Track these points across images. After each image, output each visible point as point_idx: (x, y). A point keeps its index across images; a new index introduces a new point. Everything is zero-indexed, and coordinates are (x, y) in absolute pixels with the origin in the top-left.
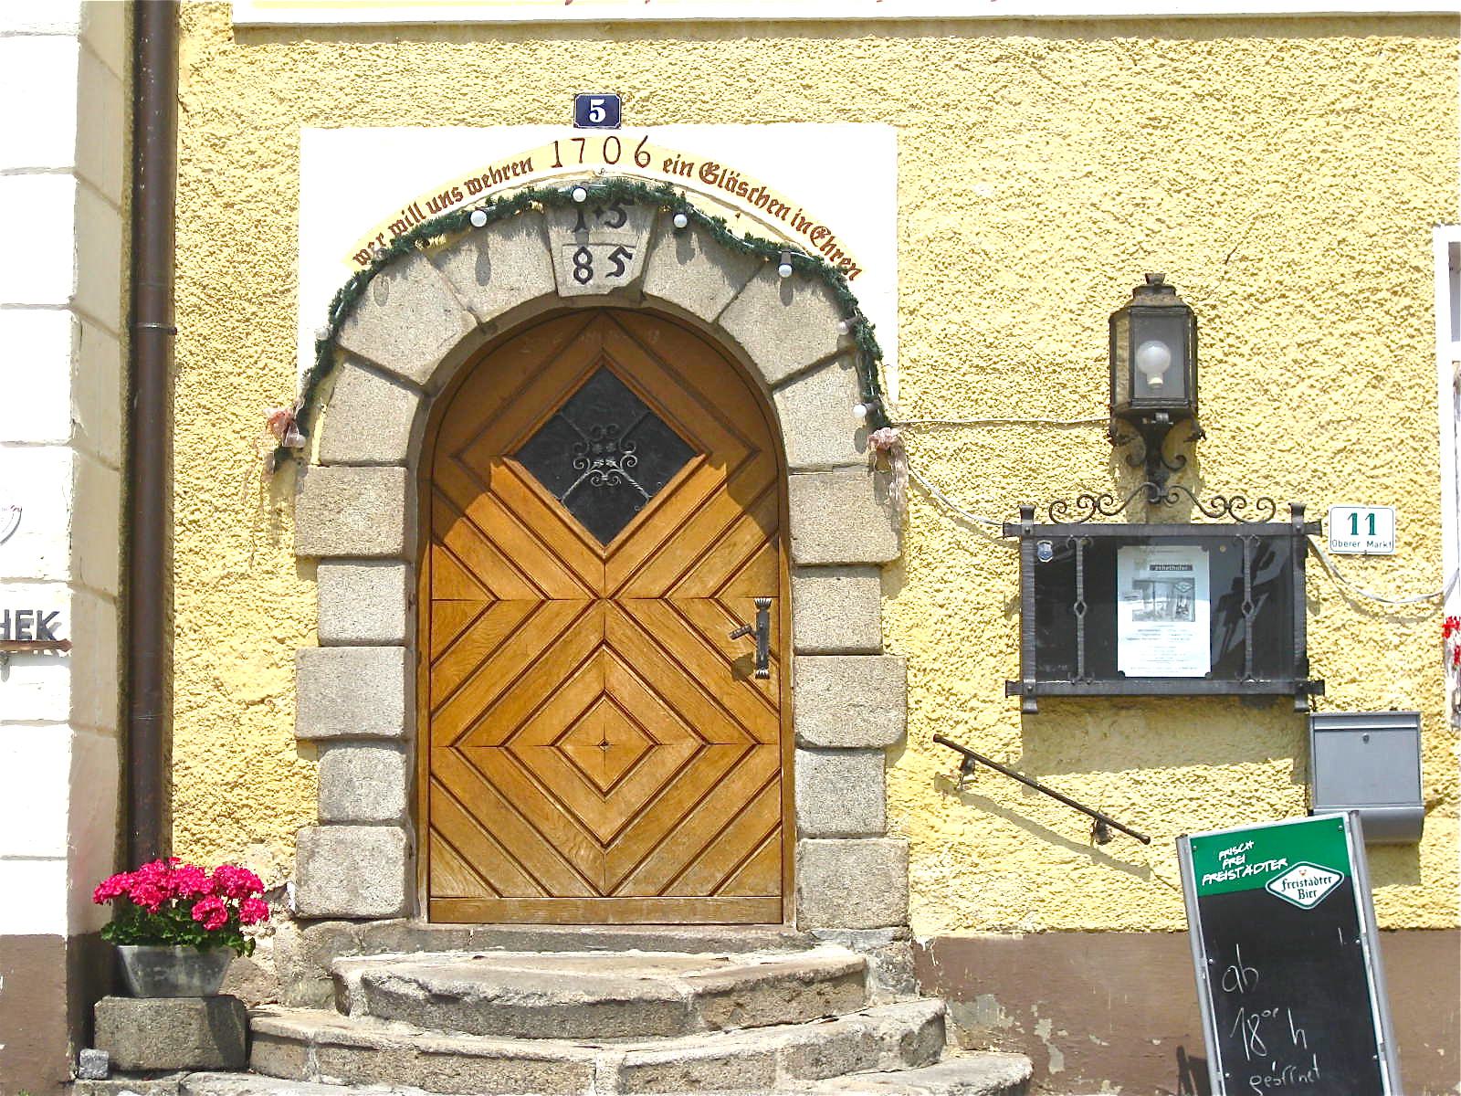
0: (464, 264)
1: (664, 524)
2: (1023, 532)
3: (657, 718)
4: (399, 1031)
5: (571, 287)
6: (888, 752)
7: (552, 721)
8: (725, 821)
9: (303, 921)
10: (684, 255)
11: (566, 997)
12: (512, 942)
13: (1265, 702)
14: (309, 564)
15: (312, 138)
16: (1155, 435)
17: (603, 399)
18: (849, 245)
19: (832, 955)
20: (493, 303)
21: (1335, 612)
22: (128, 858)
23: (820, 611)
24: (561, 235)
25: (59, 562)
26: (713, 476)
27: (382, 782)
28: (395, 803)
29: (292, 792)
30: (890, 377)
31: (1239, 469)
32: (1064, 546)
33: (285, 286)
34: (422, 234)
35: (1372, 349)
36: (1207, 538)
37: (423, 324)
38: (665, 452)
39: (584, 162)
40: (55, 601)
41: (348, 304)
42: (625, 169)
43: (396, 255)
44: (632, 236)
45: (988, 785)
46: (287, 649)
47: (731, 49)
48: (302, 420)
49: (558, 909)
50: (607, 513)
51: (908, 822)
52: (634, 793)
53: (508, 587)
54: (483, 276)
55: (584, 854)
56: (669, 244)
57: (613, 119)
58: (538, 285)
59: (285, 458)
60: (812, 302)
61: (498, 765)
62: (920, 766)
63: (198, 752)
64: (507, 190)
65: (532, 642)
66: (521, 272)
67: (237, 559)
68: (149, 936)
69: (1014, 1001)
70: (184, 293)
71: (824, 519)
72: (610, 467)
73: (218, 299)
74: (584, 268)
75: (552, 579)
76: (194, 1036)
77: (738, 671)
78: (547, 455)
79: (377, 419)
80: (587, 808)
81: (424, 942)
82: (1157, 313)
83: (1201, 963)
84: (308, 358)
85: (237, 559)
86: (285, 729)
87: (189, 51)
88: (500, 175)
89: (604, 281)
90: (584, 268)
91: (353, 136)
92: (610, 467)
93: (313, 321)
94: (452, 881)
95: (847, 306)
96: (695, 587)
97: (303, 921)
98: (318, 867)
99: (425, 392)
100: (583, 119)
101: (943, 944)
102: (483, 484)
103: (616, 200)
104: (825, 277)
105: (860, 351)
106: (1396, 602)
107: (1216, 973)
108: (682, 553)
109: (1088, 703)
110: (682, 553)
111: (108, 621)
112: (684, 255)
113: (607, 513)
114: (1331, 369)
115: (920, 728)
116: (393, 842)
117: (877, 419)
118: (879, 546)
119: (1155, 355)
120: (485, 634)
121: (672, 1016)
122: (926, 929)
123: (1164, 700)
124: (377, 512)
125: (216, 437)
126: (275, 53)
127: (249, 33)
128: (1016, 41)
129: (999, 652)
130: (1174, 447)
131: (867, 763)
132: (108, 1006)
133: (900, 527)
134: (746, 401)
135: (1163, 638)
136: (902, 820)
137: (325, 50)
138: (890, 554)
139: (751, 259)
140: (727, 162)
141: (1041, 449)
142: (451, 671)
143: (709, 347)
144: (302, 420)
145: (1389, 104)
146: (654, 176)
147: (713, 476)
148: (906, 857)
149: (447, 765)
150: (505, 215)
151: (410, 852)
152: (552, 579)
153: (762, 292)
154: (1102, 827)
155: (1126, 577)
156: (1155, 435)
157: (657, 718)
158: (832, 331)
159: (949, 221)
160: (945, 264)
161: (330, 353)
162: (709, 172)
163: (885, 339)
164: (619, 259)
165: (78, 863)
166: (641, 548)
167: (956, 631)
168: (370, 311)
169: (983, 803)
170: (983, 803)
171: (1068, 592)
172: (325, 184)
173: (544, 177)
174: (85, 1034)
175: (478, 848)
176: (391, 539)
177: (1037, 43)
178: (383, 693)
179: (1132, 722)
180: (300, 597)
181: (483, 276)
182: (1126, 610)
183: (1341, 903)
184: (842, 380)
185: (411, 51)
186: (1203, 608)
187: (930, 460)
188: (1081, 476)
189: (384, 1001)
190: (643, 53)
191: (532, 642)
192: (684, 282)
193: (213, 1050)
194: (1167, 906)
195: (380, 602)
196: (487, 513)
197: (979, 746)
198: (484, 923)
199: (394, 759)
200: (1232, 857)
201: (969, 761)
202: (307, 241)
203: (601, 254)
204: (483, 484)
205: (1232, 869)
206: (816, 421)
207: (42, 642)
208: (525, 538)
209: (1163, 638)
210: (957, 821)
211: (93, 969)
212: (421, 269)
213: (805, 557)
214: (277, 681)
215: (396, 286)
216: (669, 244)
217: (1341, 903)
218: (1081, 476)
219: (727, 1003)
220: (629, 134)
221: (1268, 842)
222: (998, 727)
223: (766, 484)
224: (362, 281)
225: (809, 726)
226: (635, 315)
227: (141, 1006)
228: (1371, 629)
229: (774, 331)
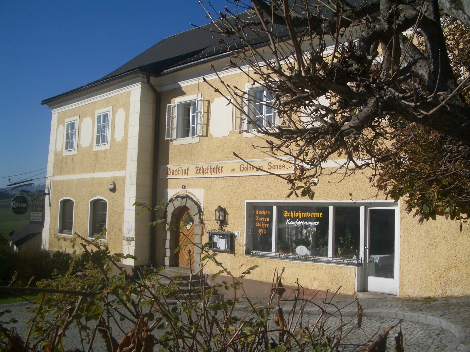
57: (185, 188)
100: (185, 186)
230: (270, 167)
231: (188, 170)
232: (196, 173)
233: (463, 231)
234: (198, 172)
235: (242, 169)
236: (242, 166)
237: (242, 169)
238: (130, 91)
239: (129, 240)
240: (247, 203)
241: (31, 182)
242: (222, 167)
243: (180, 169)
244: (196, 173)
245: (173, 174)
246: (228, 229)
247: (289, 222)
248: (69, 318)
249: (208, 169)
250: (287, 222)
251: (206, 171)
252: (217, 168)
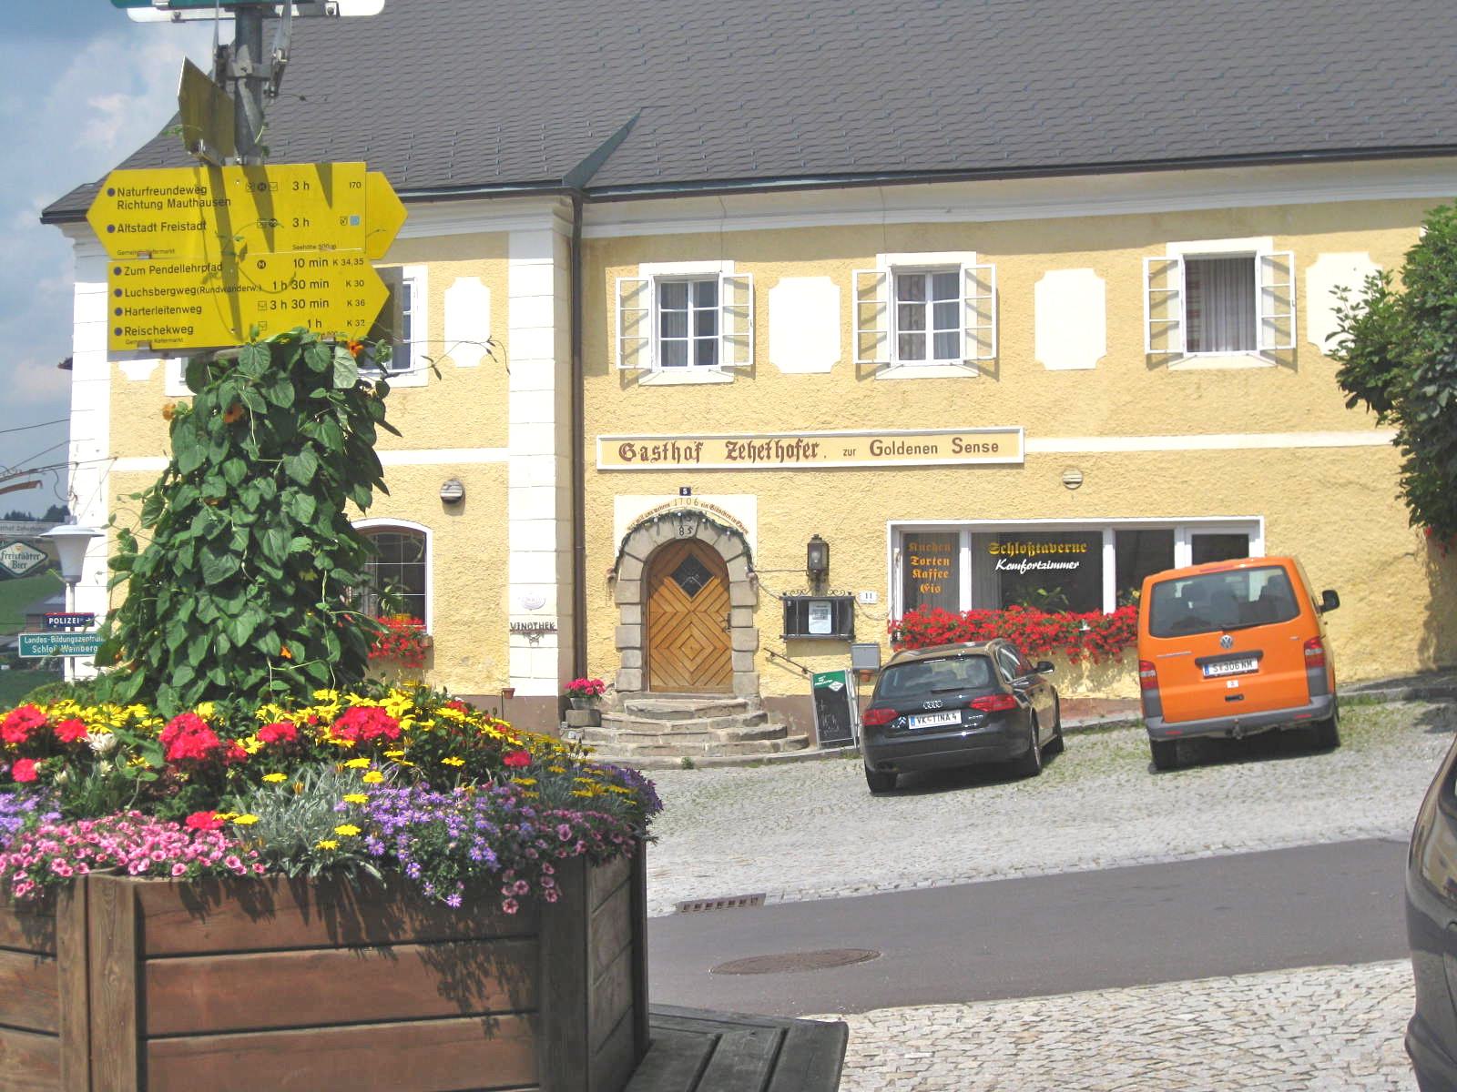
0: (654, 530)
1: (705, 593)
2: (785, 598)
3: (704, 641)
4: (633, 718)
5: (679, 537)
6: (754, 652)
7: (679, 642)
8: (715, 669)
9: (618, 692)
10: (706, 528)
11: (666, 710)
12: (666, 697)
13: (844, 640)
14: (618, 605)
15: (617, 498)
16: (819, 574)
17: (688, 562)
18: (745, 524)
19: (740, 700)
20: (661, 540)
21: (862, 618)
22: (576, 676)
23: (739, 618)
24: (676, 523)
25: (554, 610)
26: (717, 581)
27: (636, 658)
28: (639, 663)
29: (615, 660)
30: (754, 560)
31: (839, 584)
32: (793, 600)
33: (610, 538)
34: (643, 523)
35: (872, 553)
36: (832, 601)
37: (644, 546)
38: (705, 576)
39: (680, 504)
40: (554, 620)
41: (626, 540)
42: (692, 507)
43: (638, 528)
44: (693, 524)
45: (777, 660)
46: (611, 623)
47: (718, 475)
48: (616, 570)
49: (681, 689)
50: (692, 590)
51: (758, 668)
52: (699, 660)
53: (668, 609)
54: (658, 533)
55: (687, 676)
56: (702, 526)
57: (689, 493)
58: (670, 536)
59: (611, 579)
60: (736, 540)
61: (666, 653)
62: (761, 656)
63: (594, 651)
64: (664, 512)
65: (674, 623)
66: (668, 532)
67: (602, 604)
68: (576, 696)
69: (785, 712)
70: (587, 537)
71: (739, 595)
72: (693, 579)
73: (595, 539)
74: (682, 532)
75: (679, 607)
76: (587, 719)
77: (723, 630)
78: (676, 576)
79: (633, 569)
80: (688, 664)
81: (646, 697)
82: (818, 546)
83: (814, 703)
84: (617, 554)
85: (602, 604)
86: (612, 645)
87: (587, 476)
88: (661, 508)
89: (687, 535)
90: (682, 532)
91: (627, 497)
92: (693, 579)
93: (618, 544)
94: (655, 682)
95: (744, 542)
96: (713, 609)
97: (618, 692)
98: (621, 679)
99: (645, 563)
100: (682, 493)
101: (768, 699)
102: (662, 583)
103: (689, 515)
104: (737, 534)
105: (747, 553)
106: (876, 615)
107: (818, 707)
108: (710, 601)
109: (802, 640)
110: (710, 601)
111: (569, 622)
112: (706, 528)
113: (692, 590)
114: (861, 556)
115: (761, 645)
116: (638, 673)
117: (751, 570)
118: (751, 601)
119: (815, 555)
120: (662, 621)
121: (690, 715)
122: (763, 695)
123: (821, 640)
124: (633, 592)
125: (596, 572)
126: (607, 476)
127: (601, 471)
128: (785, 474)
129: (779, 628)
130: (822, 577)
131: (749, 654)
132: (568, 712)
133: (757, 596)
134: (722, 565)
135: (820, 625)
136: (757, 668)
137: (620, 476)
138: (754, 603)
139: (722, 530)
140: (716, 505)
141: (791, 577)
142: (654, 630)
143: (710, 550)
144: (616, 570)
145: (877, 489)
146: (698, 508)
147: (717, 581)
148: (758, 677)
149: (654, 652)
150: (662, 518)
151: (643, 675)
152: (679, 607)
153: (724, 538)
154: (805, 671)
155: (811, 608)
156: (819, 574)
157: (704, 641)
158: (740, 549)
159: (769, 520)
160: (767, 529)
161: (622, 552)
162: (712, 507)
163: (754, 553)
164: (689, 529)
165: (560, 679)
166: (700, 599)
167: (770, 620)
168: (631, 542)
169: (777, 664)
170: (777, 664)
171: (796, 613)
172: (622, 508)
173: (673, 509)
174: (563, 718)
175: (662, 674)
176: (637, 599)
177: (791, 474)
178: (636, 637)
179: (813, 645)
180: (616, 613)
181: (658, 533)
182: (811, 618)
183: (844, 689)
184: (743, 560)
185: (641, 476)
186: (829, 617)
187: (764, 580)
188: (799, 584)
189: (631, 712)
190: (696, 476)
191: (674, 623)
192: (706, 535)
193: (268, 711)
194: (805, 688)
195: (635, 614)
196: (663, 590)
197: (776, 651)
198: (663, 692)
199: (638, 653)
200: (821, 679)
201: (773, 654)
202: (616, 524)
203: (686, 528)
204: (662, 583)
205: (821, 681)
206: (737, 570)
207: (550, 629)
208: (672, 598)
209: (820, 625)
210: (770, 668)
211: (564, 704)
212: (643, 532)
213: (734, 604)
214: (612, 633)
215: (637, 536)
216: (702, 526)
217: (844, 689)
218: (799, 584)
219: (703, 711)
220: (693, 497)
221: (829, 676)
222: (780, 647)
223: (726, 583)
224: (629, 536)
225: (735, 645)
226: (694, 541)
227: (575, 712)
228: (870, 622)
229: (726, 548)
230: (957, 449)
231: (698, 450)
232: (729, 456)
233: (711, 1037)
234: (734, 454)
235: (877, 451)
236: (877, 444)
237: (877, 451)
238: (506, 234)
239: (532, 632)
240: (894, 528)
241: (34, 477)
242: (815, 446)
243: (670, 447)
244: (729, 456)
245: (644, 458)
246: (839, 584)
247: (1004, 565)
248: (583, 786)
249: (769, 449)
250: (999, 565)
251: (764, 453)
252: (798, 446)
